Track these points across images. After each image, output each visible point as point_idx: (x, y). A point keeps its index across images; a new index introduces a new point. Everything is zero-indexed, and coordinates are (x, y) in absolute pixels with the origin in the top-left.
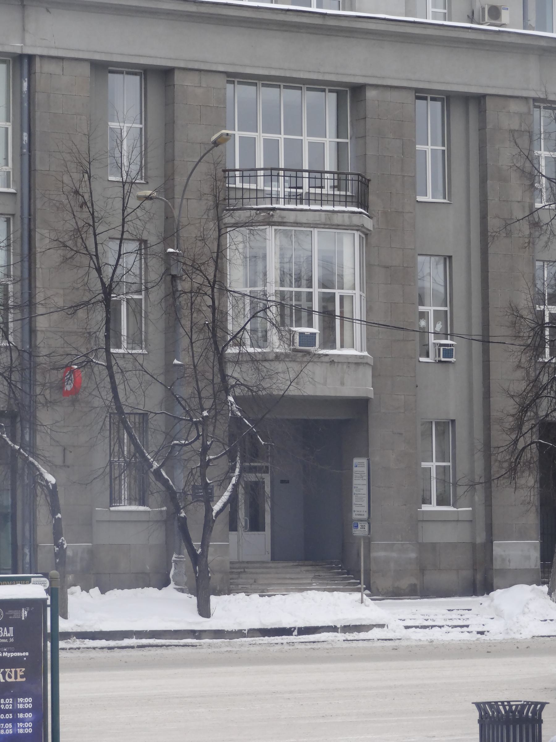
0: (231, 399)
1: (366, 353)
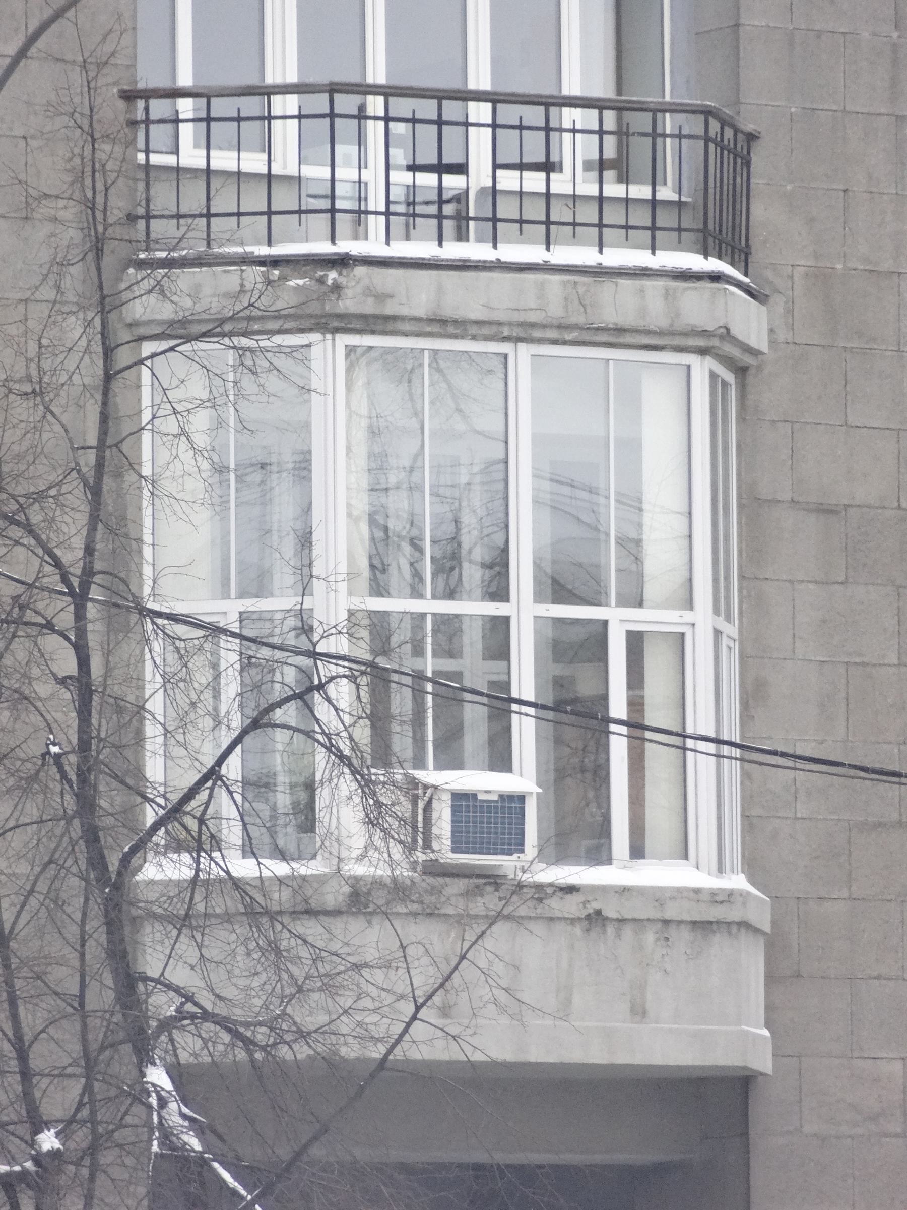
0: (158, 1077)
1: (738, 882)
